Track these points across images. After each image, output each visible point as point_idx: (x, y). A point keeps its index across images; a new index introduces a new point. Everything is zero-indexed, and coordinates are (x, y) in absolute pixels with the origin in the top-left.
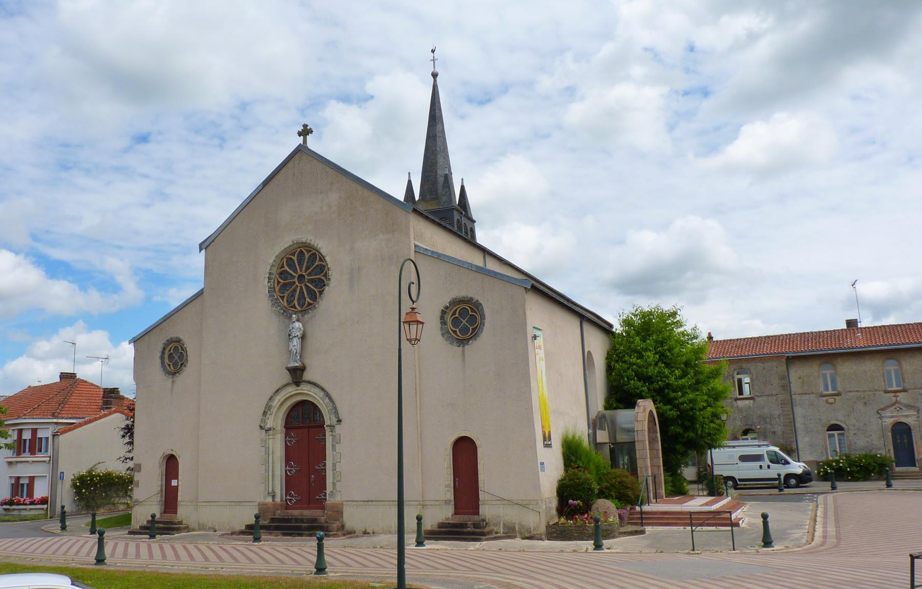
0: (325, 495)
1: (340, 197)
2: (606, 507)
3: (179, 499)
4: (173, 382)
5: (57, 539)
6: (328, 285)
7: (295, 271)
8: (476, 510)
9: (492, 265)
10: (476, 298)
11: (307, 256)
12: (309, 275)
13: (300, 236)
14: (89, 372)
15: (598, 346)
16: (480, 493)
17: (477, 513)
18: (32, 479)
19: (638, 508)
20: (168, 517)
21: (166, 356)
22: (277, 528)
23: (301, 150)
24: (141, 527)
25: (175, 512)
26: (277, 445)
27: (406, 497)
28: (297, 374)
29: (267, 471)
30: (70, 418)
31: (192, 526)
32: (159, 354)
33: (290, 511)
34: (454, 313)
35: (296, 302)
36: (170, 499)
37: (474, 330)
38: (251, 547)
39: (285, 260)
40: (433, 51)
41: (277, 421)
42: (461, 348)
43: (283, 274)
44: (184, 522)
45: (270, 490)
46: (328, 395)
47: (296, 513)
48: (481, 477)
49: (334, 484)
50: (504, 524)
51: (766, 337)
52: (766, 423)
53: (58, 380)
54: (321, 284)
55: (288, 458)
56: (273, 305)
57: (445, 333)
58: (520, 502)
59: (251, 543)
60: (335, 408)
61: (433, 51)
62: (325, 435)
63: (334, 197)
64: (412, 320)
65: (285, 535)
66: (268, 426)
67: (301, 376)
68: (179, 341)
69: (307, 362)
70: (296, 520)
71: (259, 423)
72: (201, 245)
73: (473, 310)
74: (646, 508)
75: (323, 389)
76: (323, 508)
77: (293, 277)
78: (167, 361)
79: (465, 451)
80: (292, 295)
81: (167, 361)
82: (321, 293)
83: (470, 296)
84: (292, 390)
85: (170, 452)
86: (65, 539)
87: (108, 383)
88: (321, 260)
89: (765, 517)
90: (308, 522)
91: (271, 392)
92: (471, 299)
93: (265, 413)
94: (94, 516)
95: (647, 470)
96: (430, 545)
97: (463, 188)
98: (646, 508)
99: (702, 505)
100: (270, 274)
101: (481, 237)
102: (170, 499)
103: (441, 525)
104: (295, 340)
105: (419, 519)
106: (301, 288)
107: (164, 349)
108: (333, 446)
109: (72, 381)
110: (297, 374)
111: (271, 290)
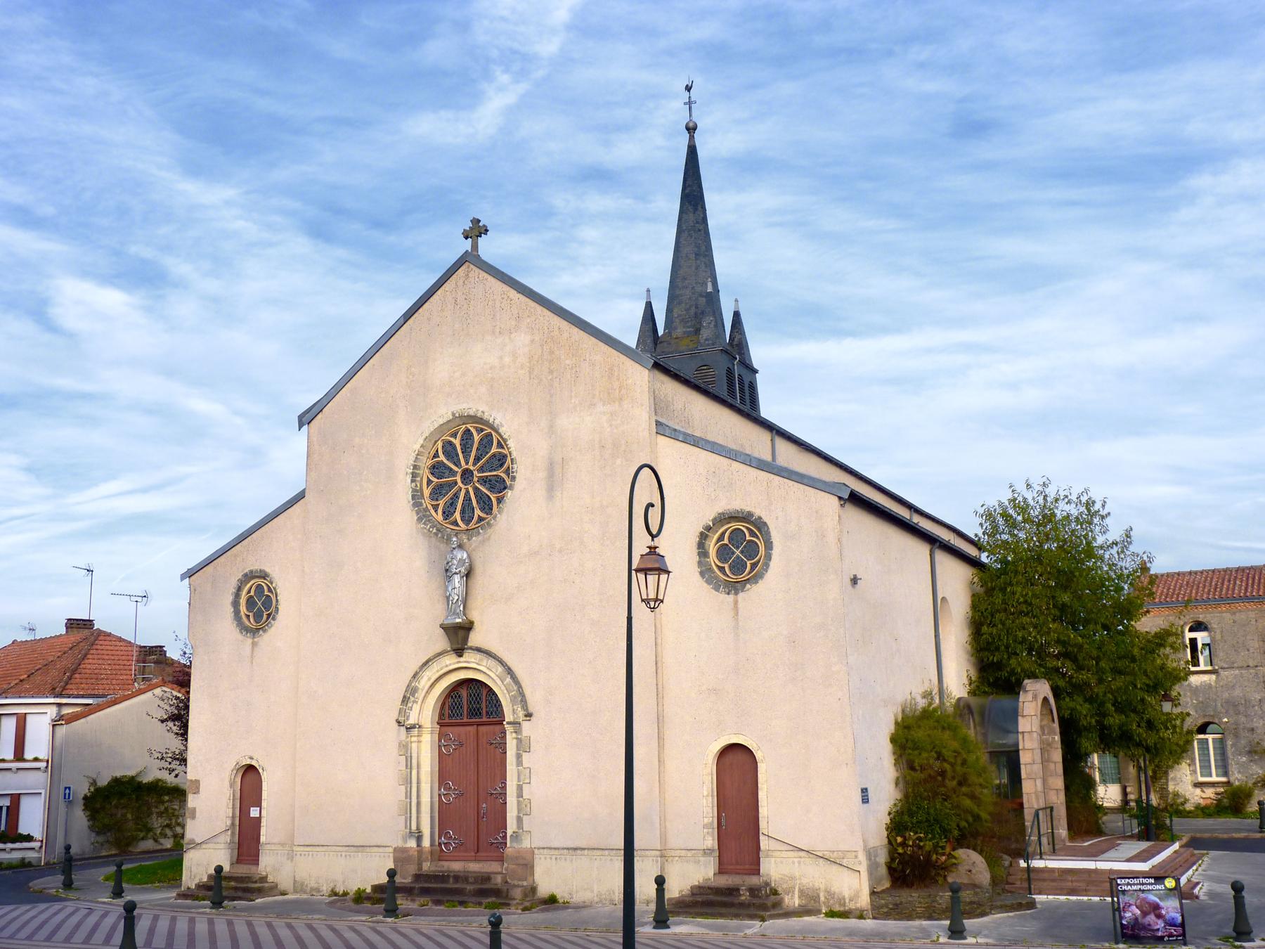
0: (505, 837)
1: (532, 341)
2: (972, 865)
3: (263, 839)
4: (254, 644)
5: (57, 906)
6: (511, 488)
7: (458, 464)
8: (754, 867)
9: (787, 455)
10: (758, 512)
11: (476, 438)
12: (481, 470)
13: (465, 406)
14: (113, 618)
15: (956, 581)
16: (762, 837)
17: (757, 872)
18: (16, 799)
19: (1023, 864)
20: (243, 870)
21: (243, 601)
22: (425, 892)
23: (470, 259)
24: (199, 886)
25: (256, 862)
26: (426, 749)
27: (637, 844)
28: (459, 635)
29: (408, 795)
30: (83, 697)
31: (282, 887)
32: (231, 598)
33: (446, 864)
34: (721, 538)
35: (457, 515)
36: (247, 837)
37: (754, 566)
38: (380, 927)
39: (440, 444)
40: (688, 88)
41: (425, 712)
42: (732, 597)
43: (437, 469)
44: (270, 879)
45: (414, 827)
46: (509, 671)
47: (456, 866)
48: (763, 811)
49: (519, 820)
50: (801, 891)
51: (1238, 570)
52: (1238, 713)
53: (62, 630)
54: (500, 486)
55: (443, 776)
56: (419, 520)
57: (705, 572)
58: (827, 855)
59: (380, 918)
60: (522, 694)
61: (688, 88)
62: (504, 737)
63: (522, 340)
64: (654, 565)
65: (438, 903)
66: (411, 721)
67: (466, 639)
68: (264, 575)
69: (475, 615)
70: (457, 878)
71: (395, 715)
72: (301, 418)
73: (752, 533)
74: (1037, 863)
75: (501, 662)
76: (501, 859)
77: (453, 473)
78: (243, 609)
79: (736, 763)
80: (452, 503)
81: (243, 609)
82: (500, 500)
83: (748, 509)
84: (451, 661)
85: (249, 762)
86: (70, 906)
87: (147, 639)
88: (500, 445)
89: (1237, 888)
90: (476, 882)
91: (415, 667)
92: (750, 514)
93: (405, 700)
94: (119, 866)
95: (1090, 906)
96: (682, 928)
97: (737, 315)
98: (1037, 863)
99: (1129, 860)
100: (415, 467)
101: (767, 410)
102: (247, 837)
103: (698, 890)
104: (457, 578)
105: (660, 881)
106: (467, 492)
107: (239, 589)
108: (519, 757)
109: (86, 632)
110: (459, 635)
111: (416, 496)
